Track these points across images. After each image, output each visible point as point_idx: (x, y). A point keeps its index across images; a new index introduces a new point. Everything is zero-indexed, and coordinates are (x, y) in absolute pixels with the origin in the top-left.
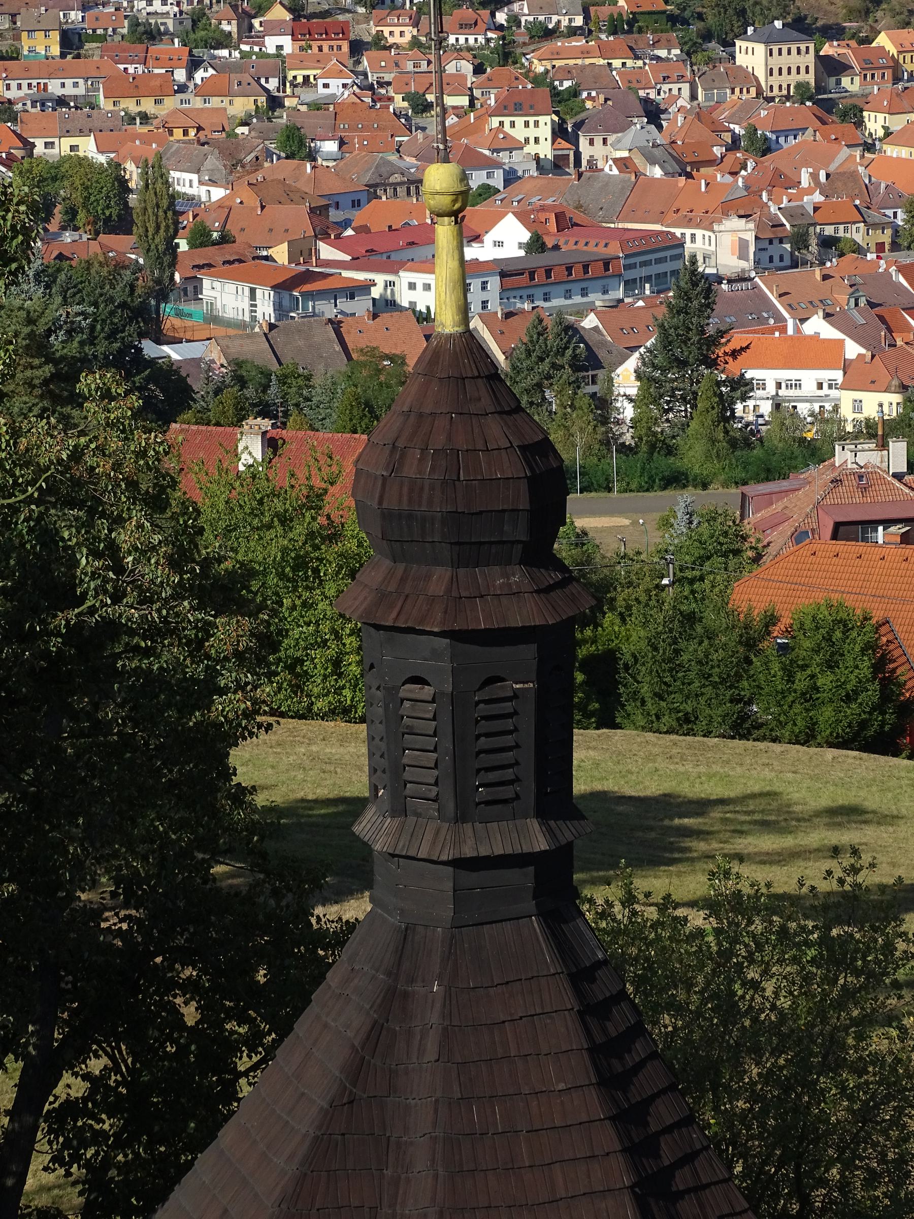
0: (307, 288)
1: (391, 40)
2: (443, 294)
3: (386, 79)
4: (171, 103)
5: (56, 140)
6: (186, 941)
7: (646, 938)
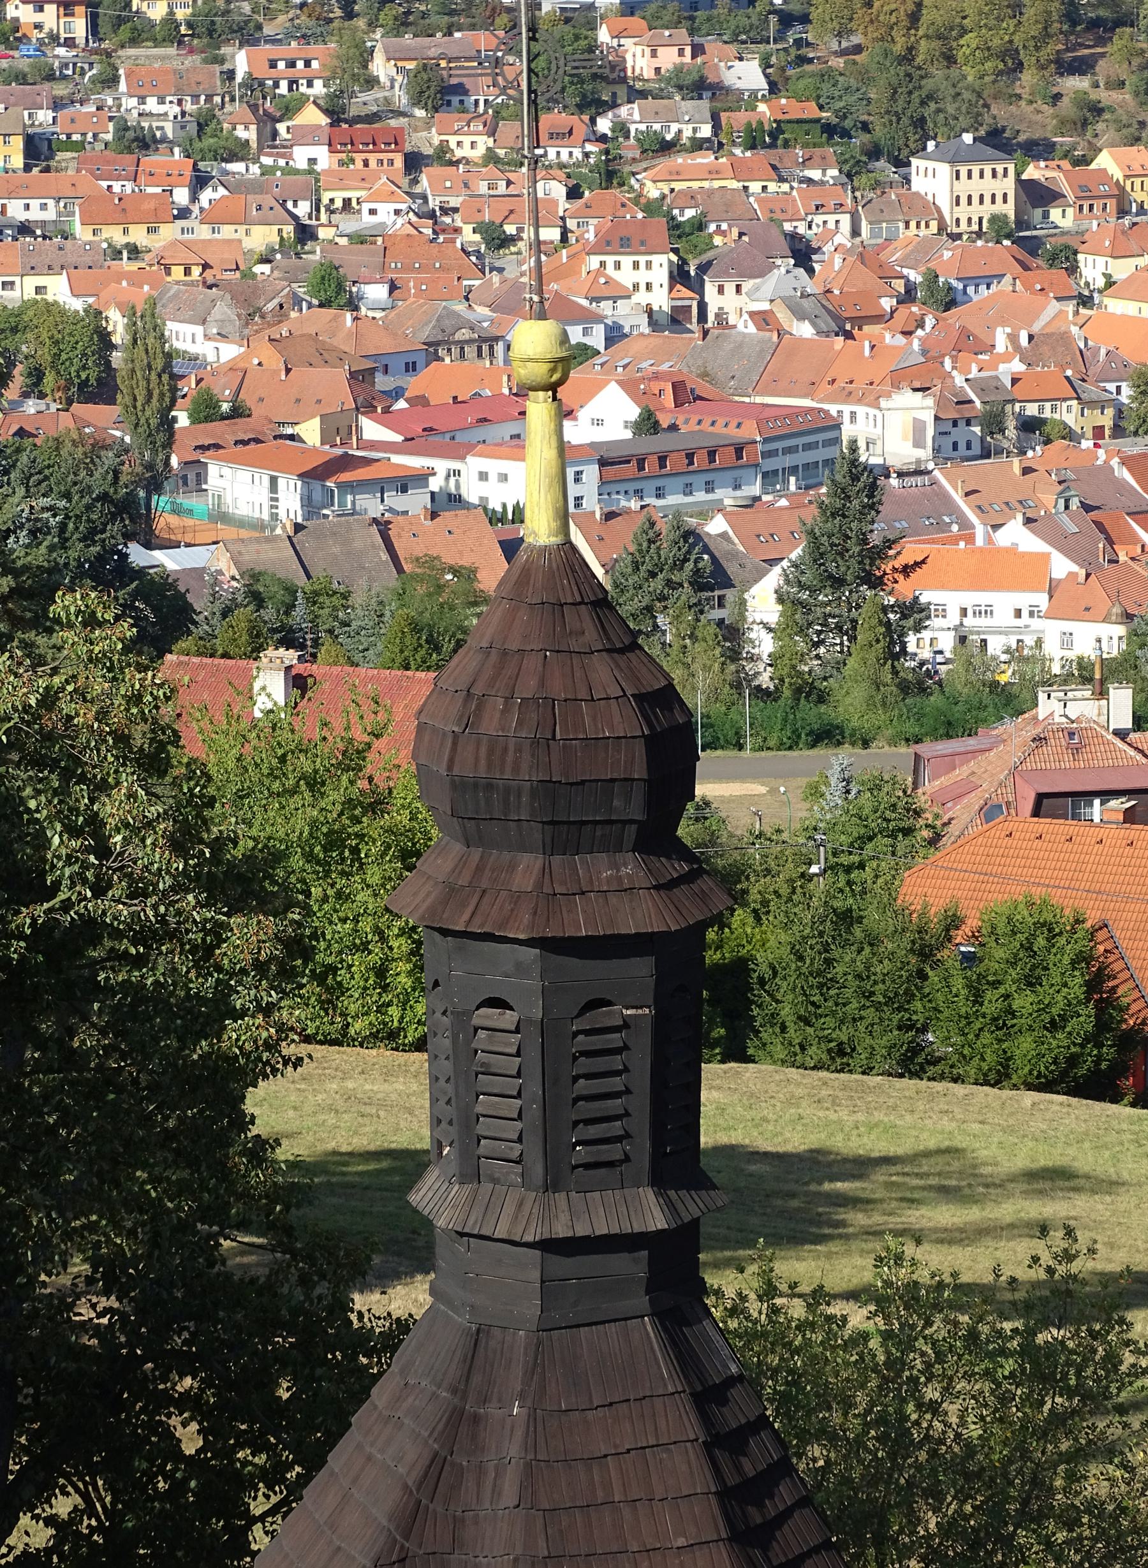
0: (345, 477)
1: (459, 153)
2: (536, 494)
3: (452, 205)
4: (169, 232)
5: (17, 280)
6: (184, 1343)
7: (791, 1343)
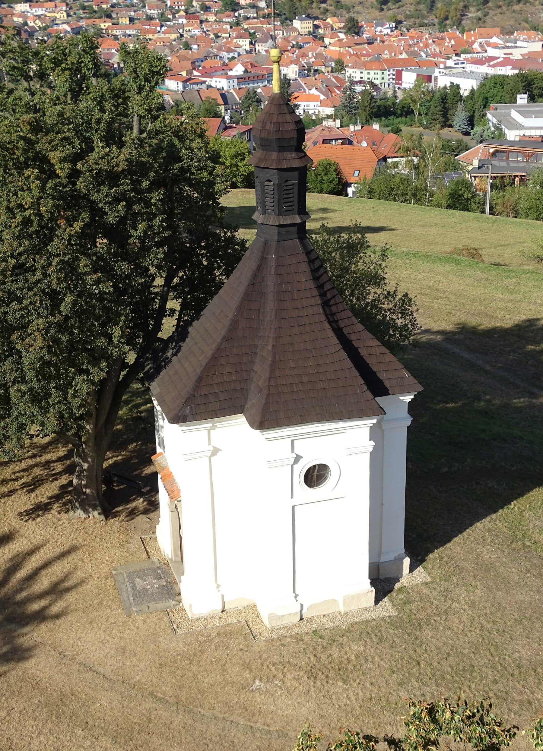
0: (191, 82)
1: (210, 20)
4: (156, 36)
